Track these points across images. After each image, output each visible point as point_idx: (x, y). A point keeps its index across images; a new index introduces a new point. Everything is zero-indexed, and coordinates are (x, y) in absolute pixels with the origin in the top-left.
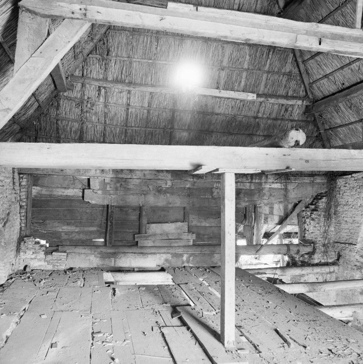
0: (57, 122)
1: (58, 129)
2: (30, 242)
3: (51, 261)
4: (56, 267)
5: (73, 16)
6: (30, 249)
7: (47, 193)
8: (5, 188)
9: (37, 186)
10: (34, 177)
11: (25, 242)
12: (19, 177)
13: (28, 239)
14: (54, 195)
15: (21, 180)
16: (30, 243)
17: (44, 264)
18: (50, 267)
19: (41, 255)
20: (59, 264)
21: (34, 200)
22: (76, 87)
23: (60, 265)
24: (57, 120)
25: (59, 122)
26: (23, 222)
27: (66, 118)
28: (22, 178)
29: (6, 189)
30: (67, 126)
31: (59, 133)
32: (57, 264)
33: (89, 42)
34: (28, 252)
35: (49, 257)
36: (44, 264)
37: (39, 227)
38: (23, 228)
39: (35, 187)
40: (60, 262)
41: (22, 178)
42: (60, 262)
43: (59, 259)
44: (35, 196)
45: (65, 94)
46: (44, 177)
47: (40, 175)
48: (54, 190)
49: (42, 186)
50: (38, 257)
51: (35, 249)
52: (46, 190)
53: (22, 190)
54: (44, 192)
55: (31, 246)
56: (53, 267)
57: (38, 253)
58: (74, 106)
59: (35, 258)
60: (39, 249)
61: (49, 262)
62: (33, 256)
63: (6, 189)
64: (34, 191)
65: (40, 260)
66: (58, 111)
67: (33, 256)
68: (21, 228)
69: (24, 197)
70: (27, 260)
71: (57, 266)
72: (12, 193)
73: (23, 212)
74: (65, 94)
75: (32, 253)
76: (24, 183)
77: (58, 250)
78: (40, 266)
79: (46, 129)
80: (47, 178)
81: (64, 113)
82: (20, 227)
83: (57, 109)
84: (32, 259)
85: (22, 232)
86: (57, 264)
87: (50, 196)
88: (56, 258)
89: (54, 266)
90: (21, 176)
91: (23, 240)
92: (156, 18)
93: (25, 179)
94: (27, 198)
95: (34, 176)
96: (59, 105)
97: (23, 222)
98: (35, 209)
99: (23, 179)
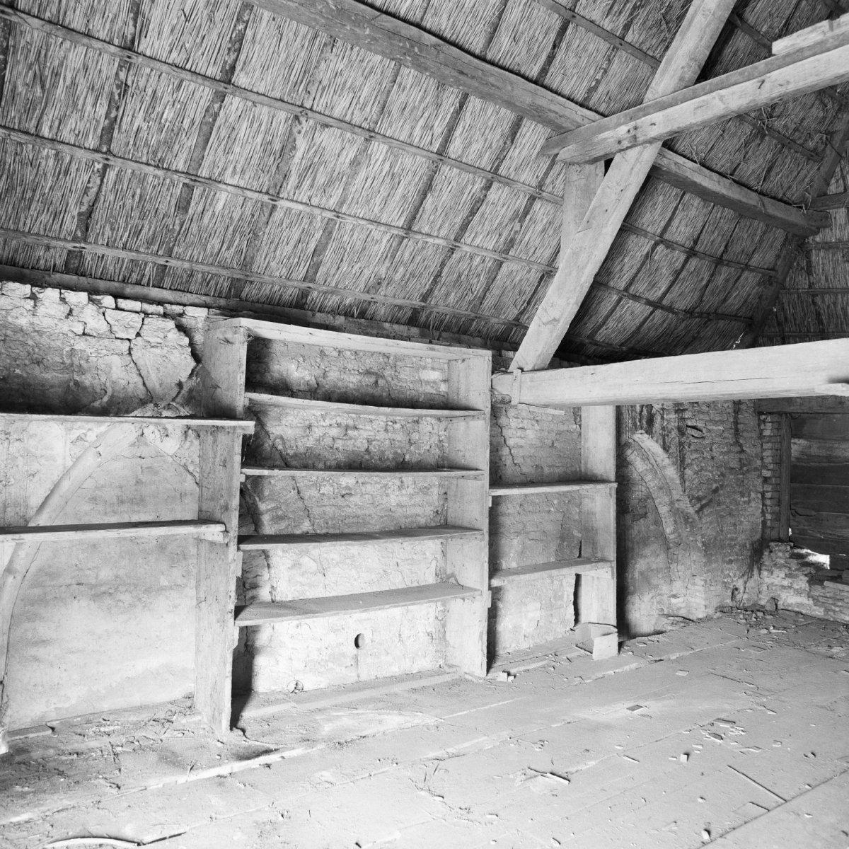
0: (813, 300)
1: (818, 314)
2: (780, 553)
3: (820, 599)
4: (832, 613)
5: (620, 147)
6: (780, 567)
7: (823, 453)
8: (706, 442)
9: (800, 437)
10: (793, 418)
11: (771, 552)
12: (759, 419)
13: (776, 546)
14: (836, 457)
15: (762, 427)
16: (780, 554)
17: (807, 602)
18: (819, 612)
19: (800, 582)
20: (837, 609)
21: (794, 467)
22: (835, 218)
23: (841, 611)
24: (814, 295)
25: (818, 300)
26: (769, 510)
27: (829, 288)
28: (764, 421)
29: (712, 444)
30: (835, 304)
31: (822, 324)
32: (833, 608)
33: (840, 116)
34: (776, 572)
35: (818, 591)
36: (807, 602)
37: (806, 523)
38: (769, 523)
39: (796, 441)
40: (840, 604)
41: (764, 421)
42: (840, 604)
43: (838, 597)
44: (797, 458)
45: (818, 239)
46: (815, 418)
47: (806, 415)
48: (837, 445)
49: (809, 437)
50: (796, 586)
51: (790, 568)
52: (818, 445)
53: (765, 446)
54: (815, 450)
55: (782, 561)
56: (824, 611)
57: (796, 577)
58: (840, 259)
59: (790, 587)
60: (796, 570)
61: (816, 601)
62: (786, 583)
63: (712, 444)
64: (794, 448)
65: (798, 592)
66: (811, 277)
67: (786, 583)
68: (764, 523)
69: (770, 460)
70: (774, 588)
71: (834, 611)
72: (729, 452)
73: (770, 489)
74: (818, 239)
75: (784, 576)
76: (767, 433)
77: (840, 577)
78: (798, 605)
79: (795, 319)
80: (820, 422)
81: (823, 278)
82: (762, 519)
83: (809, 273)
84: (783, 587)
85: (768, 531)
86: (833, 608)
87: (829, 459)
88: (831, 595)
89: (827, 610)
90: (763, 417)
91: (768, 547)
92: (750, 85)
93: (770, 424)
94: (779, 463)
95: (788, 415)
96: (809, 263)
97: (769, 510)
98: (796, 485)
99: (767, 424)
